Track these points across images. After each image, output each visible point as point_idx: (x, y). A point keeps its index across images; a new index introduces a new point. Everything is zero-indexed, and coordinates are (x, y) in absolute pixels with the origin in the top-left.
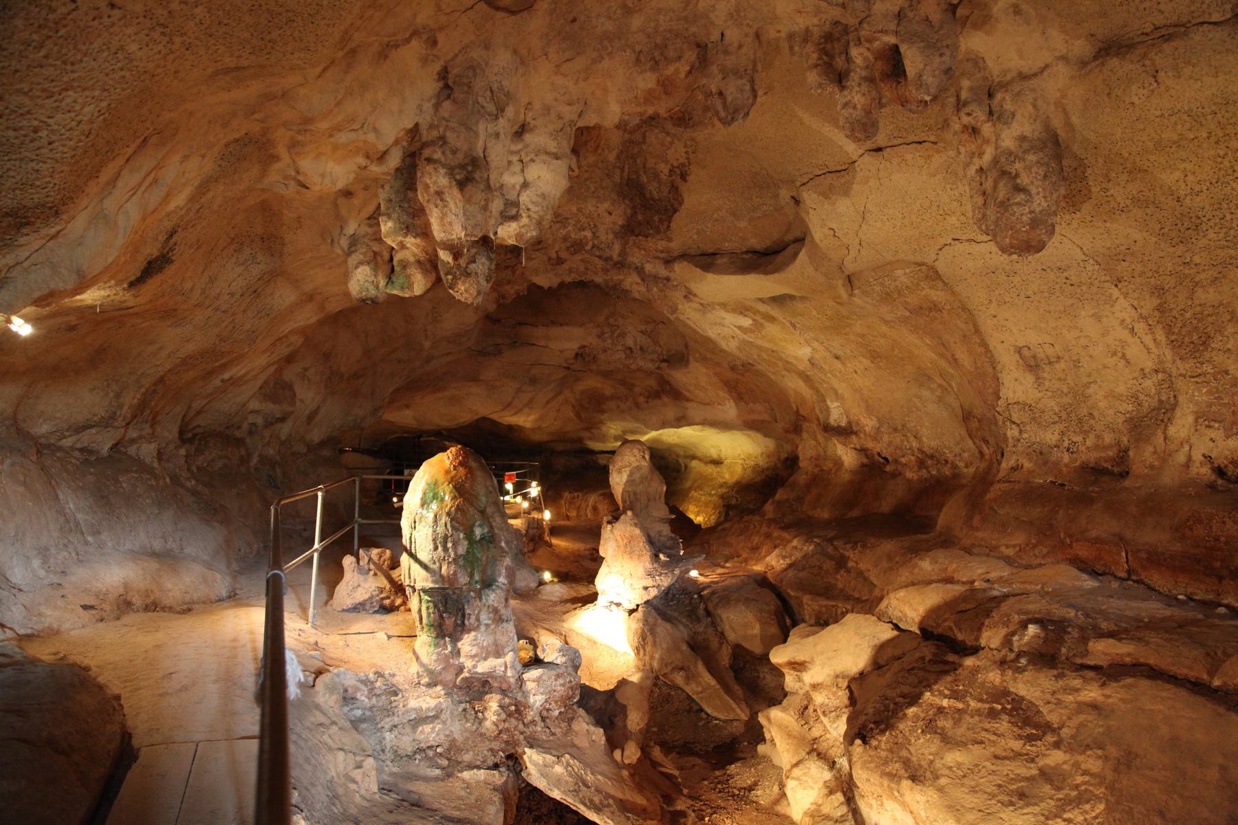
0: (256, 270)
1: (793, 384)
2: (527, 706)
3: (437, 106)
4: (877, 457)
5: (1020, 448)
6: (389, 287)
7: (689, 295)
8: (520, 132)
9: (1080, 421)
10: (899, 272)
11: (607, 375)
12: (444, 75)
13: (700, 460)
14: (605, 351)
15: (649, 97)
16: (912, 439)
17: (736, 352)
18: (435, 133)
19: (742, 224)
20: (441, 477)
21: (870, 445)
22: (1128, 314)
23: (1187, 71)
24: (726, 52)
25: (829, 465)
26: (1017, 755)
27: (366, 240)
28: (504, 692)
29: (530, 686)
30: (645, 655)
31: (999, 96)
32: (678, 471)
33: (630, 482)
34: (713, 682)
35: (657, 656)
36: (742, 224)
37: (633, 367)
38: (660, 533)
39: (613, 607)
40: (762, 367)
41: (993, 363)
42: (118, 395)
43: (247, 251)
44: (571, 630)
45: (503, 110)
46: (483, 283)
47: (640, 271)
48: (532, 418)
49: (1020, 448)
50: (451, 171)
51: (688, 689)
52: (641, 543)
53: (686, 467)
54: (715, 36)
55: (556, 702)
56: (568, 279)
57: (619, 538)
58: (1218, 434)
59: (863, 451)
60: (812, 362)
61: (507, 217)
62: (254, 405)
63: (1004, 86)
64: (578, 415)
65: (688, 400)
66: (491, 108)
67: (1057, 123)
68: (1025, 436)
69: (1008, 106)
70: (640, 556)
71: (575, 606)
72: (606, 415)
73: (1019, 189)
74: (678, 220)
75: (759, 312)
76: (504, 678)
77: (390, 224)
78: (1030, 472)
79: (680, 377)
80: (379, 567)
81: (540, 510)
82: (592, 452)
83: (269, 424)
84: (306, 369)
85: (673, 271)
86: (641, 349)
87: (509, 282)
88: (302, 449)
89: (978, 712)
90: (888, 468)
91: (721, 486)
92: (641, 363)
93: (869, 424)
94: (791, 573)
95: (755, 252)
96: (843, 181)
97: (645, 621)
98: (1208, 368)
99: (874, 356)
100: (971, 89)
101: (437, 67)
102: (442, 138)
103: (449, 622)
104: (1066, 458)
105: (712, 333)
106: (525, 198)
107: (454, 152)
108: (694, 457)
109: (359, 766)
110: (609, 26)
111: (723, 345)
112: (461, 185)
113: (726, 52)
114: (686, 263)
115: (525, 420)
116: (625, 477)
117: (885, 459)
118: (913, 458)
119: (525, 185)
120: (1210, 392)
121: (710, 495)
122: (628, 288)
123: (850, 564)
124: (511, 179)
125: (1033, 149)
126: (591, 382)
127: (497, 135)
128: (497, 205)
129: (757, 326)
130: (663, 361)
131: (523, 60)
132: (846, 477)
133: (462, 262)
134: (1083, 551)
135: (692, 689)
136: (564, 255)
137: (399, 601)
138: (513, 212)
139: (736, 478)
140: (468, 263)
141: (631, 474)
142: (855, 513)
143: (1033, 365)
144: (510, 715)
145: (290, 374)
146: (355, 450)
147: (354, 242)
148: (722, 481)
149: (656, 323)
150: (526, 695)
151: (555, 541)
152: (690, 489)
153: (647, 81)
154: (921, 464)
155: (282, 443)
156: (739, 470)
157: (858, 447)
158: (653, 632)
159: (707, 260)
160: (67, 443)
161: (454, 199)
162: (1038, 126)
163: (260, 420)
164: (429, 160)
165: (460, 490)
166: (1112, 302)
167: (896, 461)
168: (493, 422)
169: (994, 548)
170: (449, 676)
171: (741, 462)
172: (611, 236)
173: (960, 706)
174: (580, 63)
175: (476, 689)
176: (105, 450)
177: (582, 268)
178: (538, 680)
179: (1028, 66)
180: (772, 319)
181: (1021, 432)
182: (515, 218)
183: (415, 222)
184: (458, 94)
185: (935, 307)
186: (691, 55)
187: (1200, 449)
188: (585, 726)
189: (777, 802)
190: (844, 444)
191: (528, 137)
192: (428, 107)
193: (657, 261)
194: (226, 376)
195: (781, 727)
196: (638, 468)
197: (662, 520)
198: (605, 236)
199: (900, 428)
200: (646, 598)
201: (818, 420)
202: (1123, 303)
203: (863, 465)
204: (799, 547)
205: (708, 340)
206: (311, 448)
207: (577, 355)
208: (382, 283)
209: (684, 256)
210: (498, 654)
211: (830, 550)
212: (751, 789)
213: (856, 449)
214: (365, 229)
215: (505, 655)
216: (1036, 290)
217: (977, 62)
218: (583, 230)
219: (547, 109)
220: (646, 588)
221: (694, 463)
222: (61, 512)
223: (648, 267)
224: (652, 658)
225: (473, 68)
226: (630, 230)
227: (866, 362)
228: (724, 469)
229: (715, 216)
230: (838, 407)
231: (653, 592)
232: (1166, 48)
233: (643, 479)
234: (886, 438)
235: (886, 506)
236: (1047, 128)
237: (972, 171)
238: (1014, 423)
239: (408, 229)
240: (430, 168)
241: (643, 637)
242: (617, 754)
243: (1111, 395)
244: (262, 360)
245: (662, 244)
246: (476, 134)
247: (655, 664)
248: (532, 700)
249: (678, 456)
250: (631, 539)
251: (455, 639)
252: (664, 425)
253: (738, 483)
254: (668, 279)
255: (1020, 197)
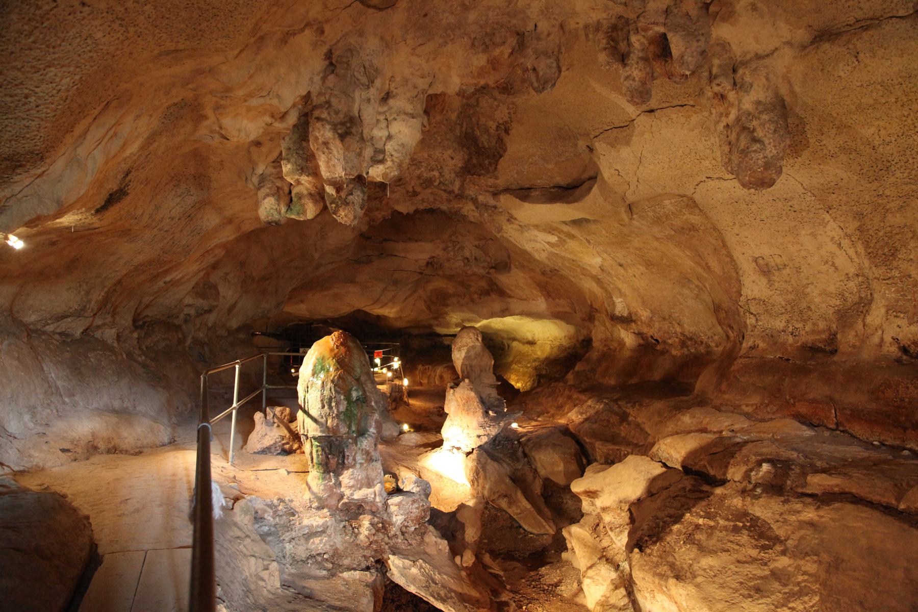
0: (190, 201)
1: (588, 285)
2: (390, 524)
3: (324, 79)
4: (650, 339)
5: (756, 332)
6: (289, 213)
7: (511, 219)
8: (386, 98)
9: (801, 312)
10: (667, 202)
11: (450, 278)
12: (329, 55)
13: (519, 341)
14: (448, 260)
15: (481, 72)
16: (676, 325)
17: (546, 261)
18: (322, 99)
19: (550, 166)
20: (327, 354)
21: (645, 330)
22: (837, 233)
23: (880, 53)
24: (538, 39)
25: (614, 345)
26: (754, 560)
27: (271, 178)
28: (373, 513)
29: (393, 509)
30: (478, 486)
31: (741, 71)
32: (503, 349)
33: (467, 357)
34: (529, 506)
35: (487, 487)
36: (550, 166)
37: (469, 272)
38: (489, 395)
39: (455, 450)
40: (565, 272)
41: (736, 269)
42: (88, 293)
43: (183, 186)
44: (424, 467)
45: (373, 82)
46: (358, 210)
47: (475, 201)
48: (394, 310)
49: (756, 332)
50: (334, 127)
51: (510, 511)
52: (475, 403)
53: (509, 346)
54: (530, 27)
55: (412, 521)
56: (421, 207)
57: (459, 399)
58: (903, 322)
59: (640, 334)
60: (602, 269)
61: (376, 161)
62: (189, 300)
63: (744, 64)
64: (429, 308)
65: (510, 297)
66: (364, 80)
67: (784, 91)
68: (760, 323)
69: (748, 79)
70: (474, 413)
71: (427, 449)
72: (449, 308)
73: (755, 140)
74: (503, 163)
75: (563, 231)
76: (373, 503)
77: (289, 166)
78: (764, 350)
79: (504, 280)
80: (281, 421)
81: (401, 379)
82: (439, 335)
83: (199, 315)
84: (227, 274)
85: (499, 201)
86: (476, 259)
87: (377, 209)
88: (224, 333)
89: (725, 528)
90: (658, 348)
91: (535, 361)
92: (476, 269)
93: (644, 314)
94: (586, 425)
95: (560, 187)
96: (625, 134)
97: (479, 461)
98: (896, 273)
99: (648, 264)
100: (720, 66)
101: (324, 49)
102: (328, 102)
103: (333, 461)
104: (791, 340)
105: (528, 247)
106: (389, 147)
107: (337, 113)
108: (514, 339)
109: (266, 568)
110: (452, 19)
111: (536, 256)
112: (342, 137)
113: (538, 39)
114: (508, 195)
115: (389, 312)
116: (463, 354)
117: (656, 340)
118: (677, 340)
119: (390, 137)
120: (897, 291)
121: (527, 367)
122: (466, 213)
123: (631, 418)
124: (379, 133)
125: (766, 110)
126: (439, 284)
127: (369, 100)
128: (368, 152)
129: (562, 242)
130: (492, 268)
131: (388, 45)
132: (627, 354)
133: (343, 194)
134: (803, 409)
135: (513, 511)
136: (418, 189)
137: (296, 446)
138: (381, 157)
139: (546, 354)
140: (347, 195)
141: (468, 352)
142: (634, 381)
143: (766, 271)
144: (378, 530)
145: (215, 278)
146: (263, 334)
147: (263, 179)
148: (535, 357)
149: (486, 239)
150: (390, 515)
151: (411, 402)
152: (512, 362)
153: (480, 60)
154: (683, 344)
155: (209, 329)
156: (548, 348)
157: (636, 331)
158: (484, 469)
159: (524, 193)
160: (50, 328)
161: (337, 148)
162: (770, 94)
163: (193, 312)
164: (318, 119)
165: (341, 363)
166: (824, 224)
167: (664, 342)
168: (366, 313)
169: (737, 407)
170: (333, 502)
171: (549, 343)
172: (453, 175)
173: (712, 523)
174: (430, 47)
175: (353, 511)
176: (78, 334)
177: (431, 199)
178: (399, 505)
179: (762, 49)
180: (572, 237)
181: (757, 320)
182: (382, 162)
183: (308, 165)
184: (340, 70)
185: (693, 228)
186: (512, 41)
187: (890, 333)
188: (434, 539)
189: (576, 595)
190: (626, 330)
191: (391, 102)
192: (317, 79)
193: (487, 194)
194: (168, 279)
195: (579, 539)
196: (473, 347)
197: (491, 386)
198: (448, 175)
199: (667, 317)
200: (479, 444)
201: (607, 312)
202: (832, 225)
203: (640, 345)
204: (592, 406)
205: (525, 252)
206: (230, 332)
207: (428, 263)
208: (283, 210)
209: (507, 190)
210: (369, 485)
211: (616, 408)
212: (557, 585)
213: (634, 333)
214: (271, 170)
215: (374, 486)
216: (768, 215)
217: (724, 46)
218: (433, 170)
219: (406, 81)
220: (479, 436)
221: (515, 344)
222: (46, 380)
223: (481, 198)
224: (483, 488)
225: (351, 50)
226: (467, 170)
227: (642, 269)
228: (537, 348)
229: (530, 160)
230: (622, 302)
231: (485, 439)
232: (865, 36)
233: (477, 355)
234: (657, 325)
235: (657, 375)
236: (777, 95)
237: (721, 127)
238: (752, 314)
239: (302, 170)
240: (318, 125)
241: (477, 473)
242: (458, 560)
243: (824, 293)
244: (194, 267)
245: (491, 181)
246: (353, 99)
247: (486, 493)
248: (394, 519)
249: (503, 338)
250: (468, 400)
251: (338, 474)
252: (492, 315)
253: (547, 358)
254: (495, 207)
255: (757, 146)
